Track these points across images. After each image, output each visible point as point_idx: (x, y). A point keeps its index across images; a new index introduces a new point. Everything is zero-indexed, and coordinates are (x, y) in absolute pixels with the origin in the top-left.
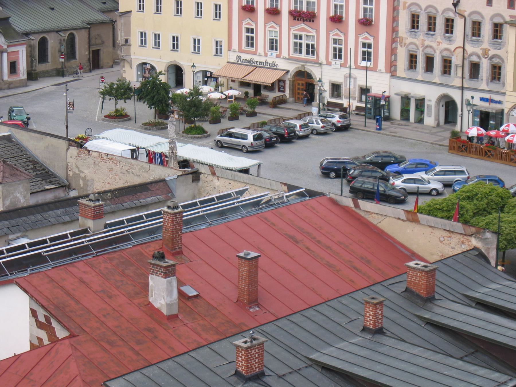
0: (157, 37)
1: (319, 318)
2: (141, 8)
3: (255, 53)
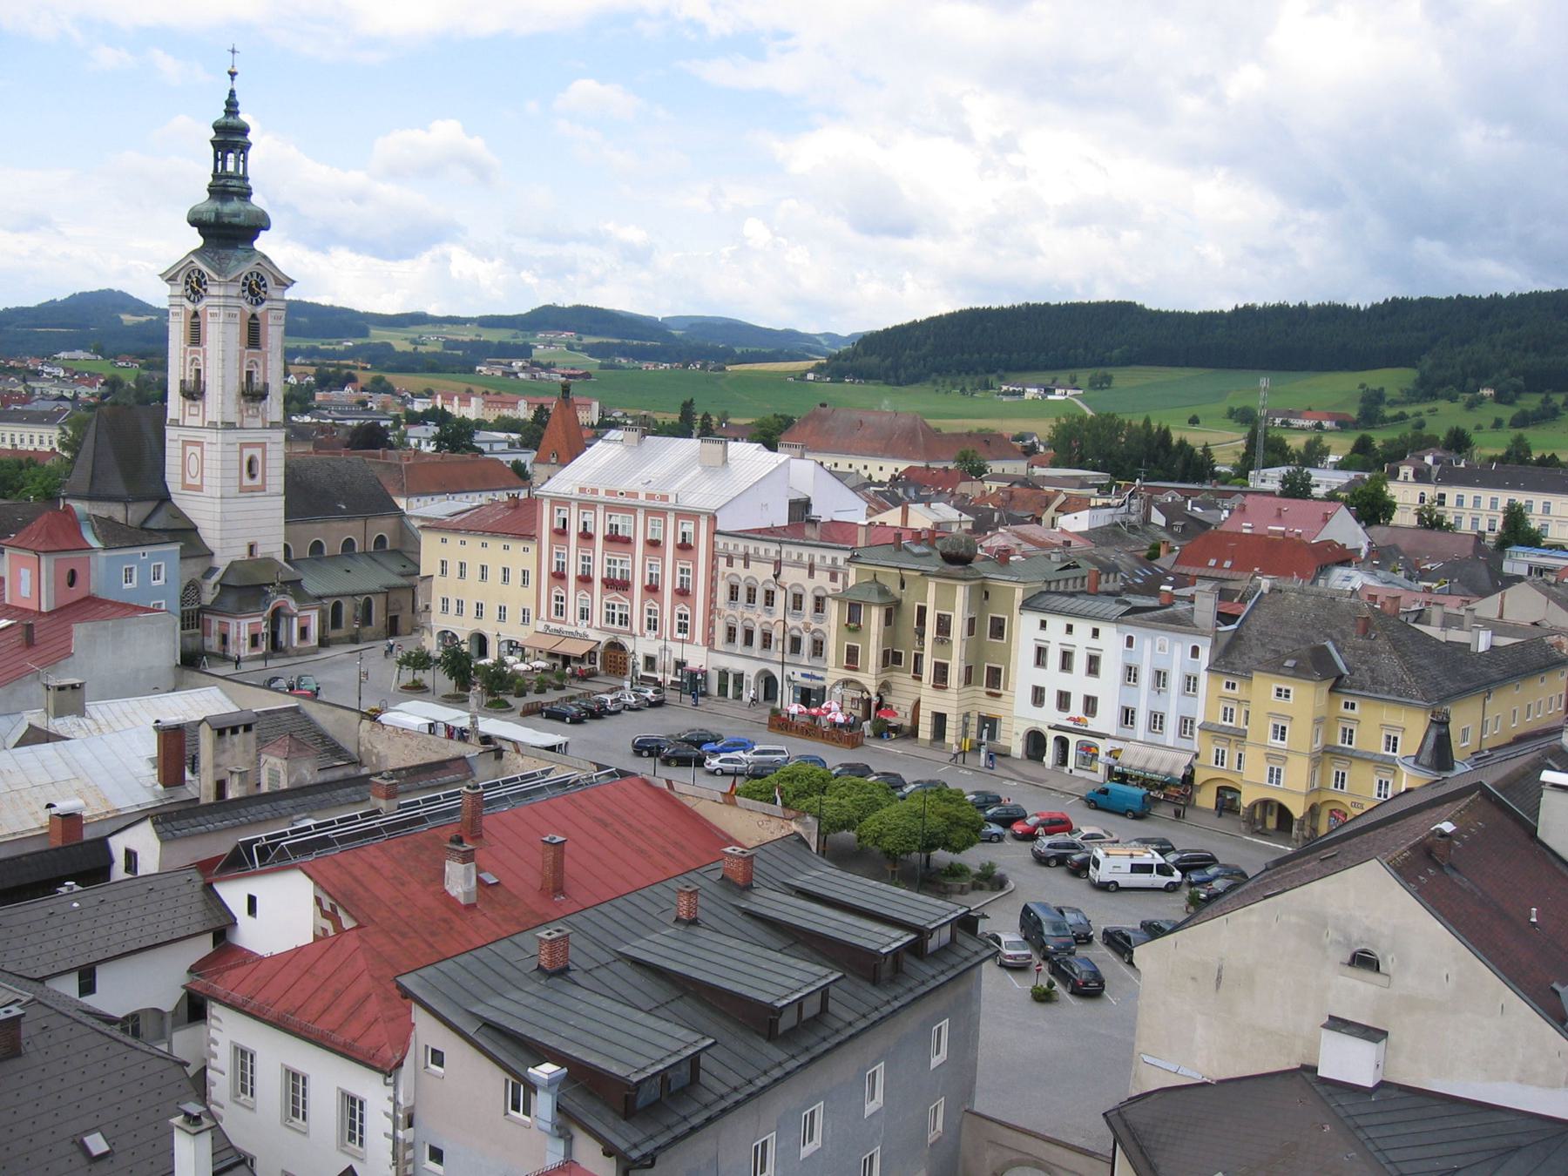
0: (460, 603)
1: (629, 908)
3: (564, 623)
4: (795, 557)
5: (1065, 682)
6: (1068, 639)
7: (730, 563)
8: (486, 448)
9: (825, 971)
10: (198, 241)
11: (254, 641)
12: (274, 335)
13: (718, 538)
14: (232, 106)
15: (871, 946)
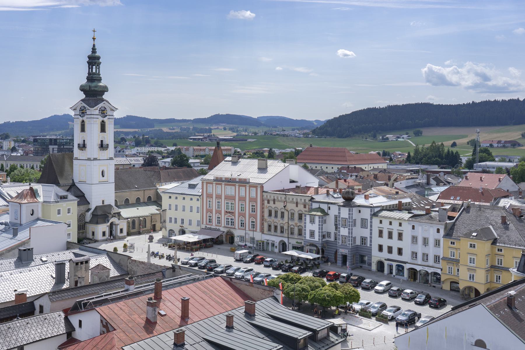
0: (176, 219)
1: (210, 323)
2: (170, 209)
3: (212, 225)
4: (291, 199)
5: (390, 243)
6: (390, 227)
7: (268, 203)
8: (192, 165)
9: (277, 345)
10: (83, 96)
11: (104, 234)
12: (110, 128)
13: (264, 193)
14: (94, 50)
15: (296, 336)
